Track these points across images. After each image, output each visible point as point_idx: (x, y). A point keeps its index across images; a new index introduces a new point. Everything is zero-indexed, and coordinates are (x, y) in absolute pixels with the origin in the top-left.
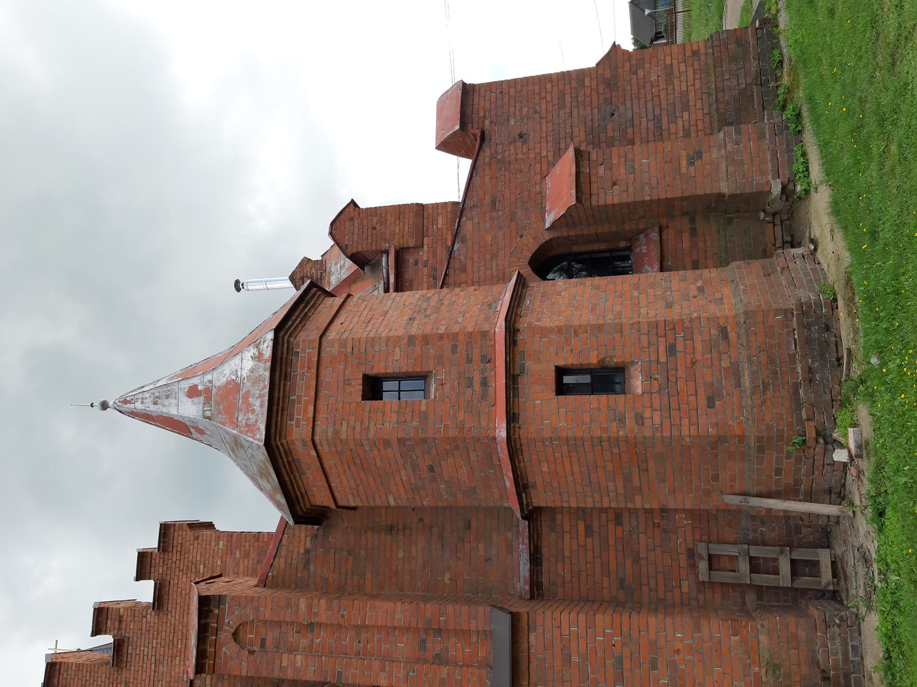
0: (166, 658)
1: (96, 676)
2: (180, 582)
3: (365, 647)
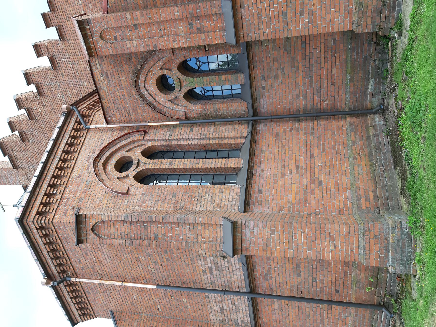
0: (76, 61)
1: (47, 75)
2: (68, 25)
3: (164, 32)
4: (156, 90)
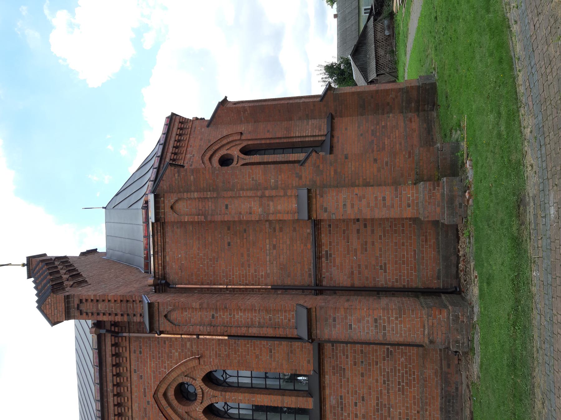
4: (173, 397)
